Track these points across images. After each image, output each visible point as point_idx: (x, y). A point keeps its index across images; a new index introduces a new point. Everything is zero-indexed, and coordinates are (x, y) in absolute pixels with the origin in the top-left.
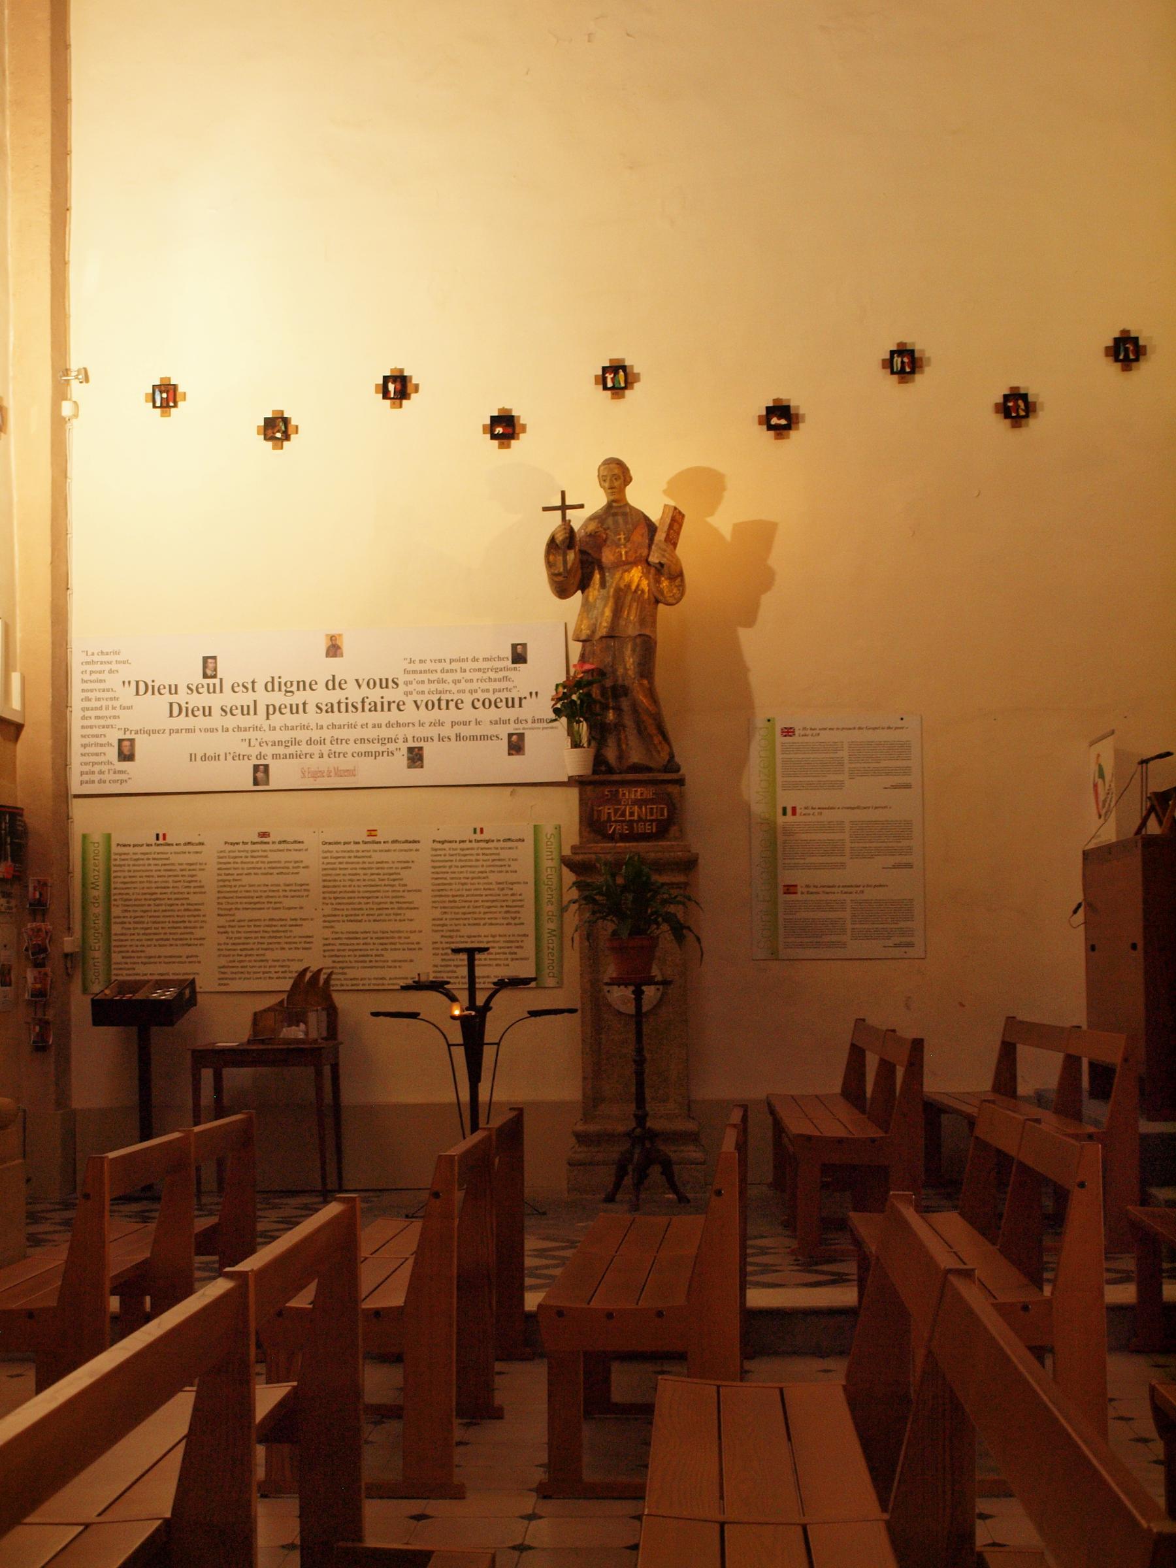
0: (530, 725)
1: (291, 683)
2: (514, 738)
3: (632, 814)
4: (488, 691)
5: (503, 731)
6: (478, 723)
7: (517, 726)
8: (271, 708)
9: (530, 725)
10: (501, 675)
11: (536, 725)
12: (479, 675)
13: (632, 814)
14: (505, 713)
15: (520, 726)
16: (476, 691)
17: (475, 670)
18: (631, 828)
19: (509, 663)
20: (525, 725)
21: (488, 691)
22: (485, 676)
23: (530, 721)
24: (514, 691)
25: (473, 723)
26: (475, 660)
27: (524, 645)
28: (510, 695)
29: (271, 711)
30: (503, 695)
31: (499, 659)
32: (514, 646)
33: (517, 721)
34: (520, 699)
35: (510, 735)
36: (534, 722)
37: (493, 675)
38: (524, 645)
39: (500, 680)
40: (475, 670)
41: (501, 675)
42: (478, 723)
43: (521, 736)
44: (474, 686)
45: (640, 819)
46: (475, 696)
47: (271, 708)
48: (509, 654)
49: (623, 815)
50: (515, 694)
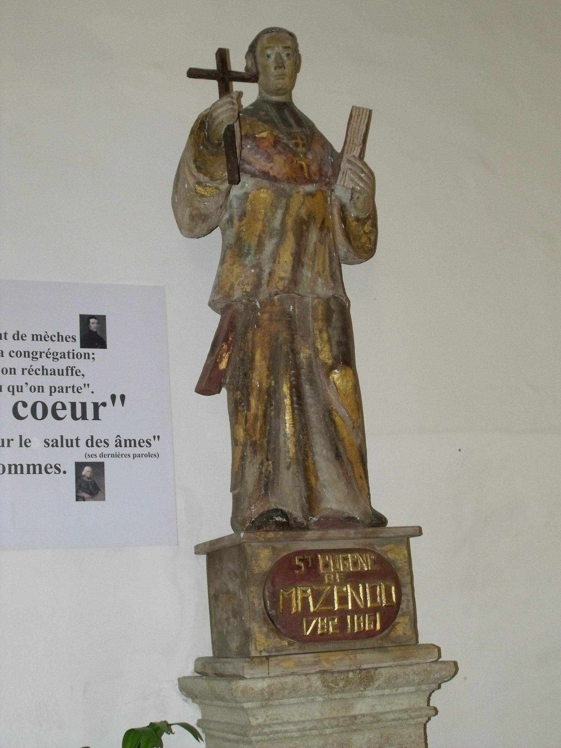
0: (112, 449)
1: (57, 353)
2: (87, 471)
3: (343, 600)
4: (41, 389)
5: (68, 458)
6: (24, 443)
7: (91, 451)
8: (53, 388)
9: (112, 449)
10: (62, 364)
11: (123, 450)
12: (26, 362)
13: (343, 600)
14: (69, 428)
15: (95, 450)
16: (20, 389)
17: (19, 354)
18: (343, 624)
19: (76, 346)
20: (106, 451)
21: (41, 389)
22: (37, 365)
23: (112, 443)
24: (85, 390)
25: (15, 444)
26: (18, 336)
27: (102, 319)
28: (78, 398)
29: (53, 390)
30: (67, 398)
31: (60, 338)
32: (85, 320)
33: (92, 442)
34: (96, 406)
35: (79, 466)
36: (119, 444)
37: (49, 364)
38: (102, 319)
39: (61, 373)
40: (19, 354)
41: (62, 364)
42: (24, 443)
43: (98, 468)
44: (17, 380)
45: (356, 609)
46: (19, 397)
47: (53, 388)
48: (76, 331)
49: (329, 601)
50: (87, 397)
